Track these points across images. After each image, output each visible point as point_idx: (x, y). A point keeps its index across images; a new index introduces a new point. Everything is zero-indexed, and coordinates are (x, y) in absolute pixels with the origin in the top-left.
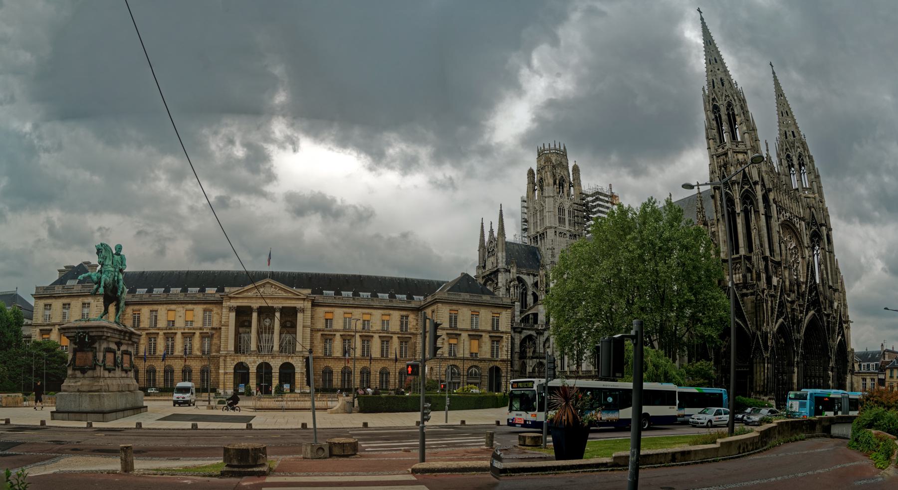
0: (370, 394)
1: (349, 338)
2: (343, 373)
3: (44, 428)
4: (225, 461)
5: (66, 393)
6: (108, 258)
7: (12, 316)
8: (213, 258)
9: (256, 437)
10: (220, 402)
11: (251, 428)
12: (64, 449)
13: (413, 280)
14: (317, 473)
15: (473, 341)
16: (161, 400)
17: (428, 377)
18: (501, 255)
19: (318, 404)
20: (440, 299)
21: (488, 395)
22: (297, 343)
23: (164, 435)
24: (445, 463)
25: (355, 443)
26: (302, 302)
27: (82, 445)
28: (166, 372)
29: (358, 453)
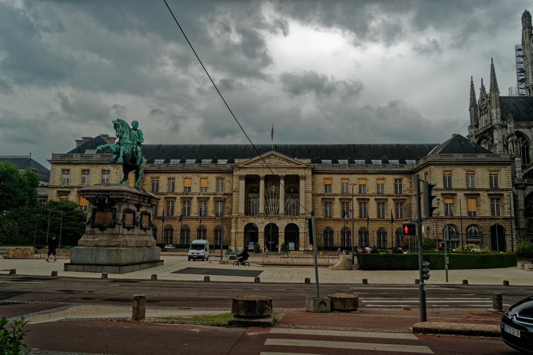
0: (369, 253)
1: (347, 201)
2: (343, 233)
3: (54, 279)
4: (233, 312)
5: (83, 247)
6: (125, 132)
7: (26, 177)
8: (222, 134)
9: (263, 290)
10: (231, 258)
11: (259, 282)
12: (75, 298)
13: (404, 146)
14: (318, 327)
15: (470, 200)
16: (177, 255)
17: (425, 236)
18: (495, 112)
19: (320, 261)
20: (432, 161)
21: (492, 254)
22: (301, 207)
23: (178, 286)
24: (448, 324)
25: (355, 298)
26: (303, 170)
27: (95, 294)
28: (182, 230)
29: (358, 309)
